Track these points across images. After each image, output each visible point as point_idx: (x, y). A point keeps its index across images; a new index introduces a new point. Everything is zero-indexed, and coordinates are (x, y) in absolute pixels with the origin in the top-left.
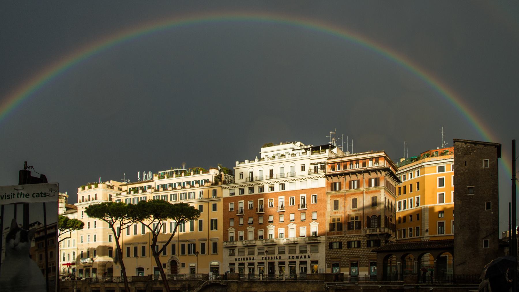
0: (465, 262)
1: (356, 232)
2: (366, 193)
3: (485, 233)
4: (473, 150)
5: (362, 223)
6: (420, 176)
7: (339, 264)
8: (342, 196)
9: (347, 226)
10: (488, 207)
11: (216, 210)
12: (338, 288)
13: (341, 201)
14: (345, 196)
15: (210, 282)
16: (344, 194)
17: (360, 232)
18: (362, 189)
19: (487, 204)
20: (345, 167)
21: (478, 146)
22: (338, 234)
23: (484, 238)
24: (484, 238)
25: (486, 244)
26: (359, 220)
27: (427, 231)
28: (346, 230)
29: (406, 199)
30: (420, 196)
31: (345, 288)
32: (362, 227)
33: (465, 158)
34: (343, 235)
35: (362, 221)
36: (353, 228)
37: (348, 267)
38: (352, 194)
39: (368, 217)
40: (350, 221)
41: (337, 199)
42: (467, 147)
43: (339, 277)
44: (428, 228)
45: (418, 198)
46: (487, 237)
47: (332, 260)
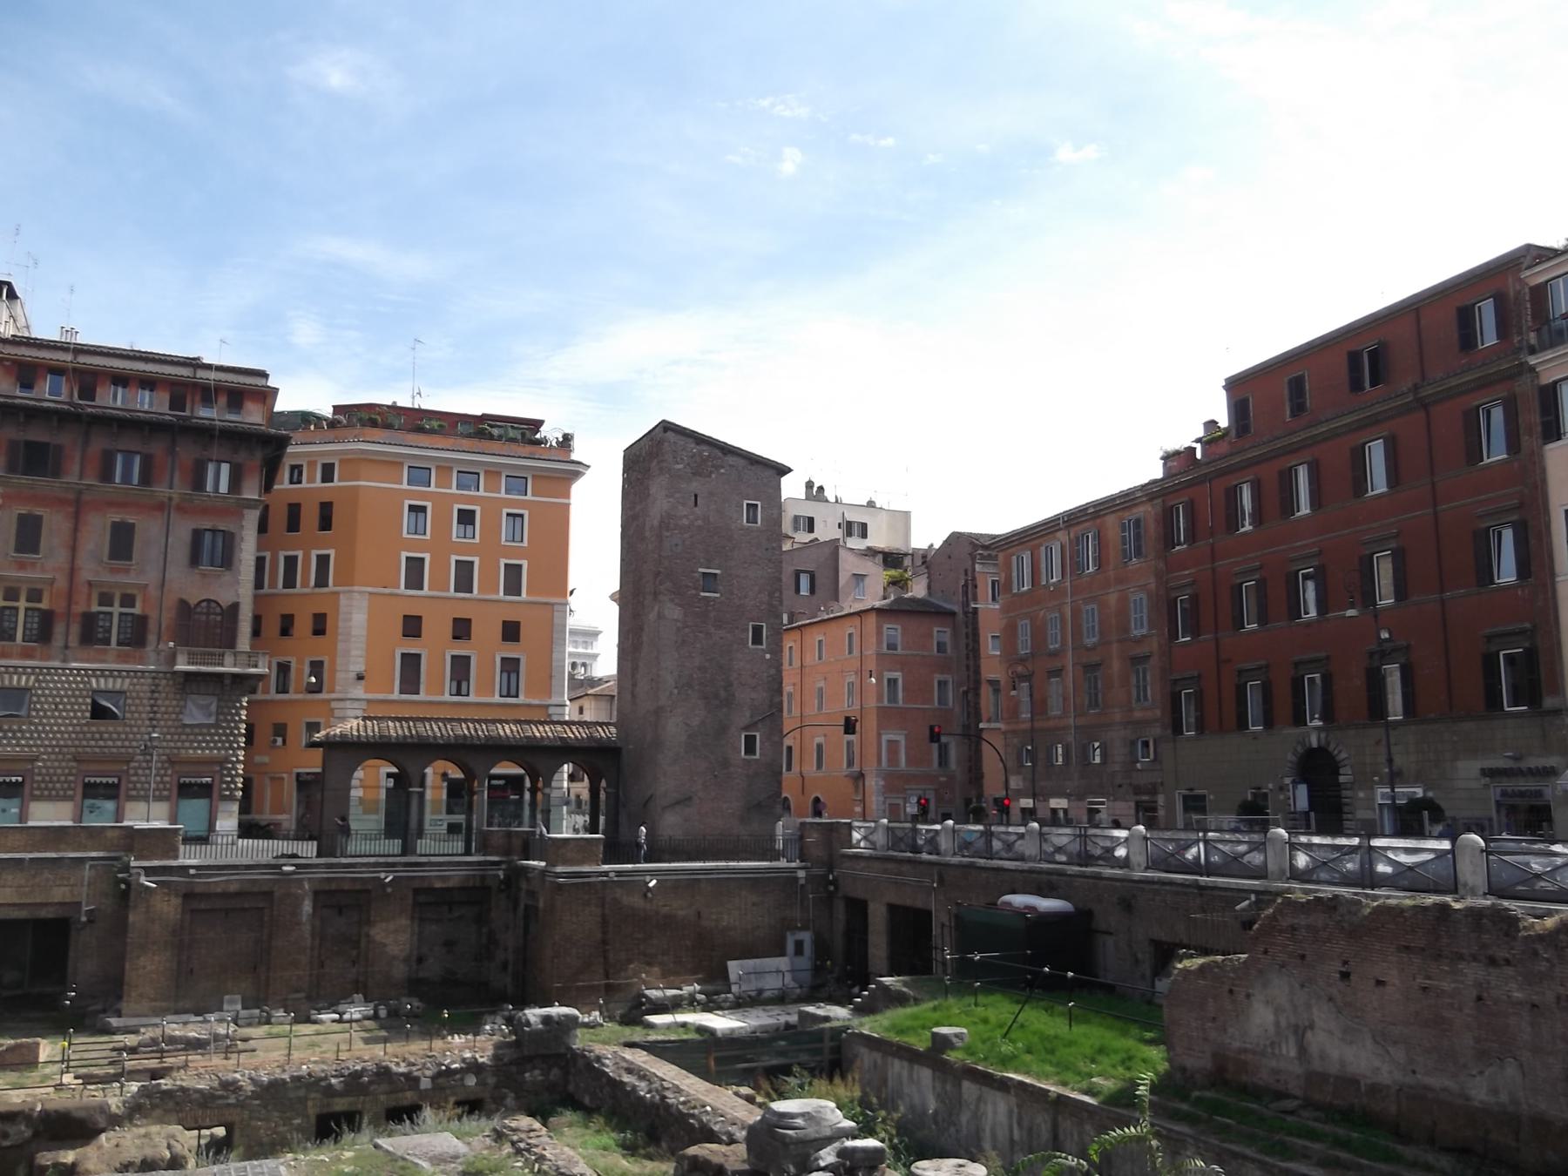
0: (690, 799)
1: (123, 658)
2: (180, 509)
3: (748, 714)
4: (717, 467)
5: (152, 625)
6: (336, 483)
7: (116, 787)
8: (61, 502)
9: (75, 629)
10: (757, 639)
11: (322, 504)
12: (198, 890)
13: (55, 524)
14: (77, 507)
15: (406, 960)
16: (71, 496)
17: (141, 661)
18: (161, 490)
19: (754, 628)
20: (88, 392)
21: (731, 459)
22: (27, 655)
23: (746, 728)
24: (746, 728)
25: (750, 749)
26: (137, 610)
27: (360, 677)
28: (74, 640)
29: (300, 554)
30: (332, 552)
31: (233, 888)
32: (152, 638)
33: (695, 486)
34: (57, 664)
35: (153, 615)
36: (107, 642)
37: (70, 798)
38: (112, 504)
39: (183, 603)
40: (95, 608)
41: (38, 511)
42: (700, 453)
43: (1509, 923)
44: (360, 668)
45: (323, 561)
46: (752, 726)
47: (84, 767)
